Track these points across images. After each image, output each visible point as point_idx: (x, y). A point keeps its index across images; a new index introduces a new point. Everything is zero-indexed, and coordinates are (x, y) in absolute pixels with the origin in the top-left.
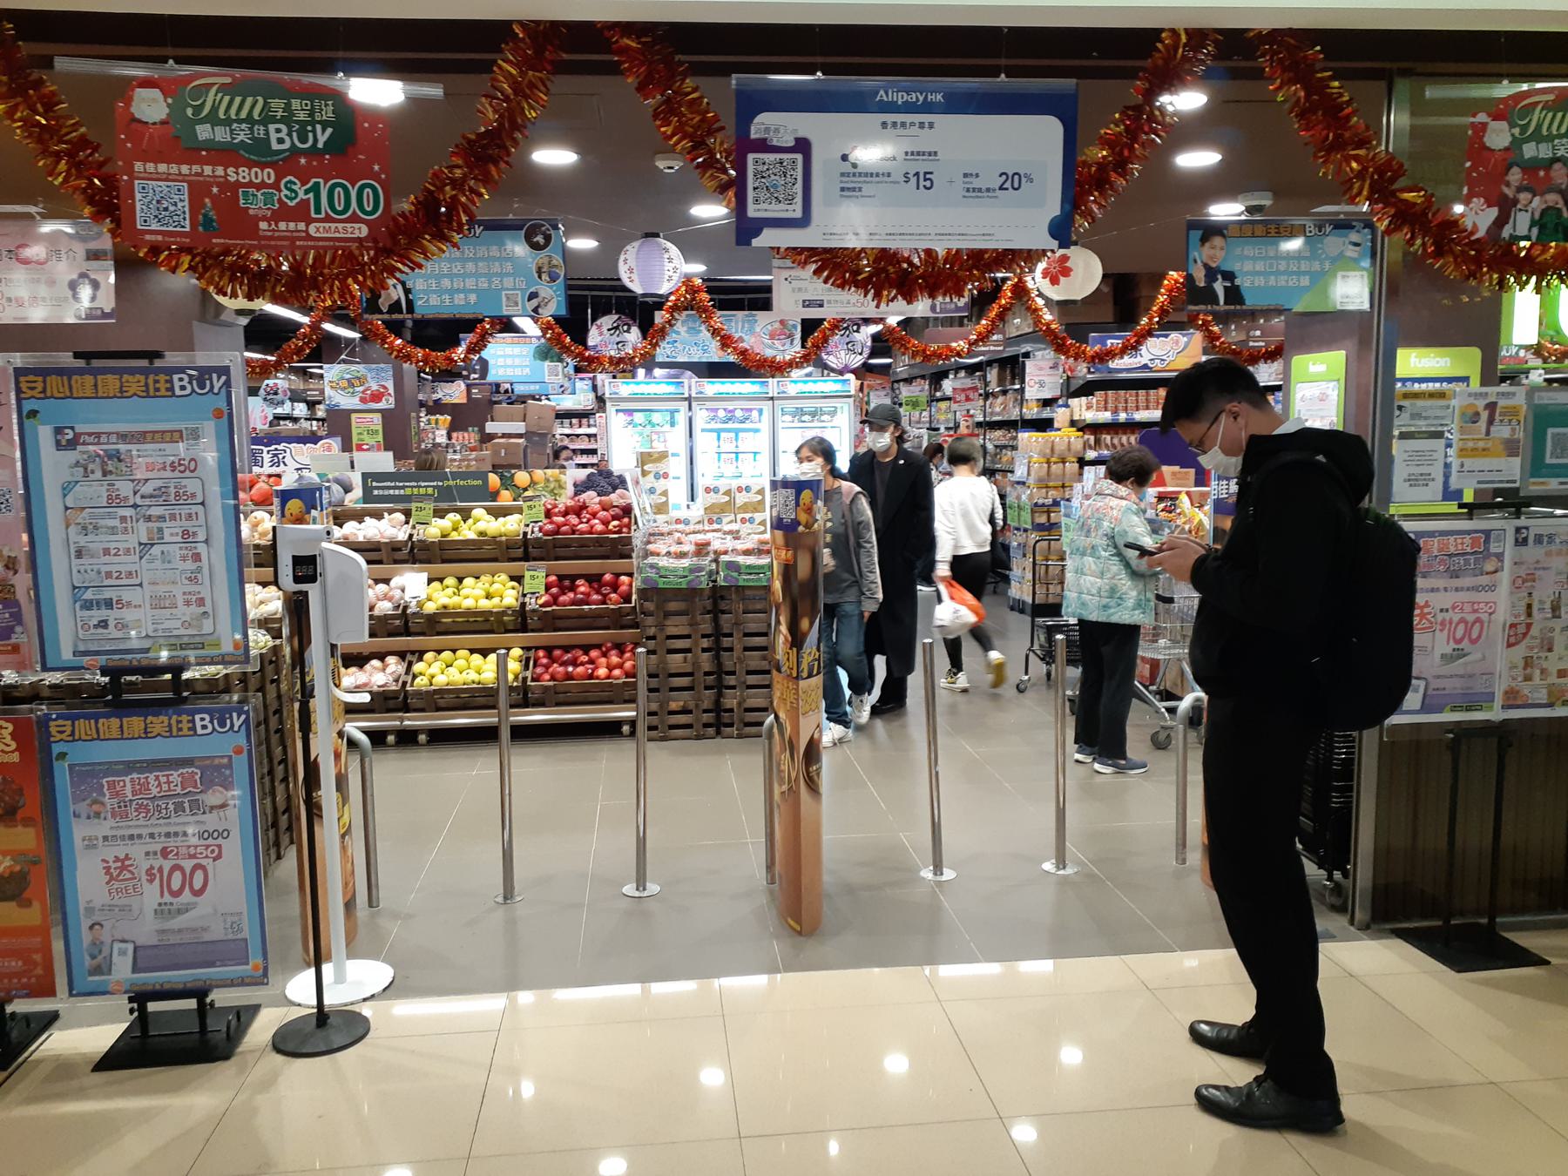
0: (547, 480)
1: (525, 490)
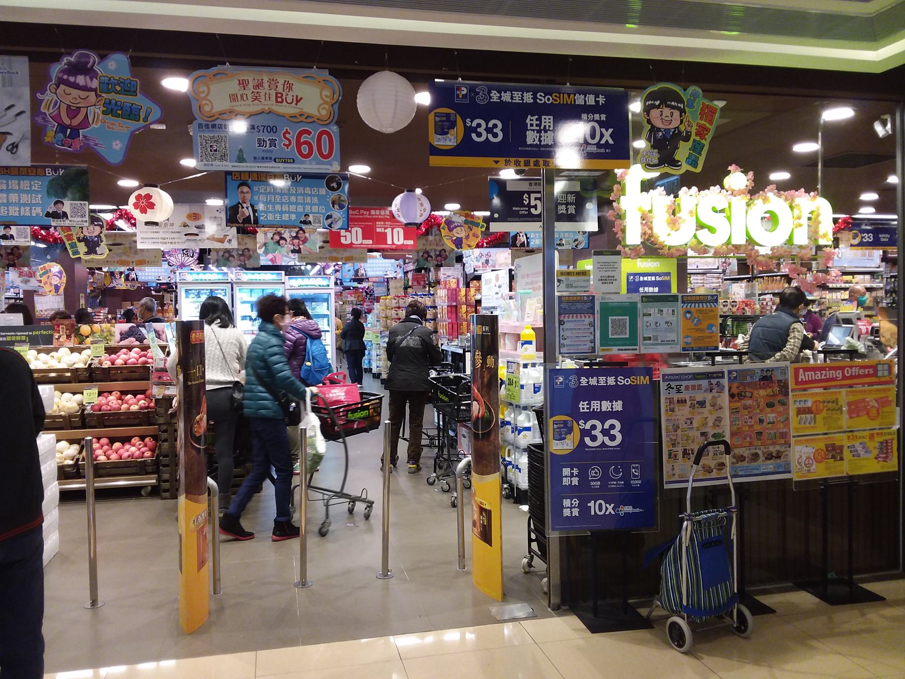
0: (103, 331)
1: (87, 337)
